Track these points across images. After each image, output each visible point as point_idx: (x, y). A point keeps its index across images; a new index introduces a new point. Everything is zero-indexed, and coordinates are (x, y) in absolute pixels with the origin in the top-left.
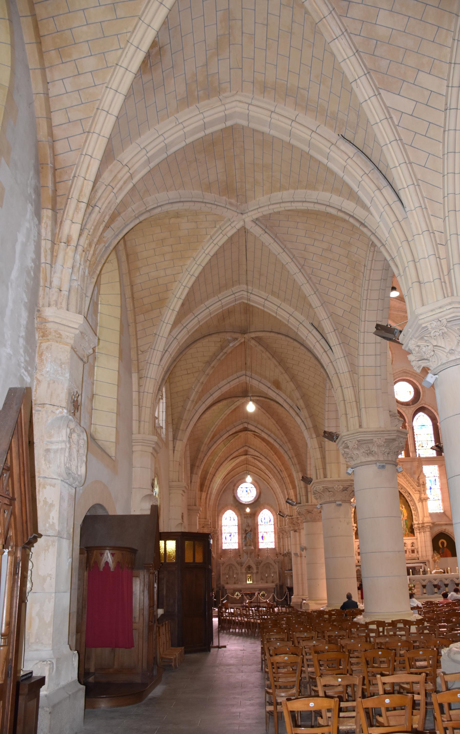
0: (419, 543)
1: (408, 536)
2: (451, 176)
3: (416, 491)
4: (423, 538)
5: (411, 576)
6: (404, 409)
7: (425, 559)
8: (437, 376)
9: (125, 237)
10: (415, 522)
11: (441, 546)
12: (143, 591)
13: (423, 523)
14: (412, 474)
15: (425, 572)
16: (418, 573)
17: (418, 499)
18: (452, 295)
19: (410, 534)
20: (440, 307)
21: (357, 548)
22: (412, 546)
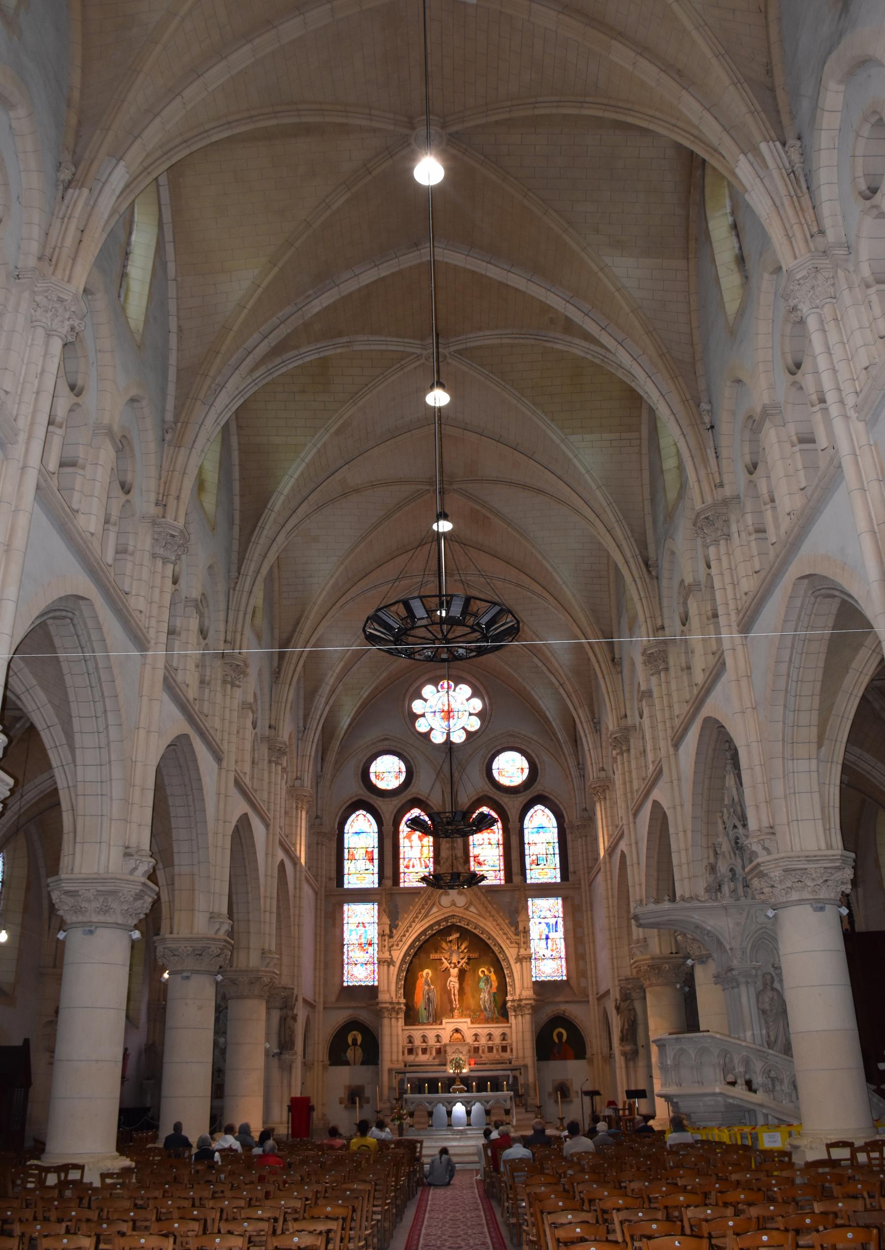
1: (497, 1022)
3: (511, 943)
4: (520, 1025)
7: (521, 1062)
9: (12, 665)
11: (556, 1040)
12: (85, 543)
13: (520, 1000)
17: (515, 957)
19: (501, 1018)
21: (406, 1040)
22: (504, 1039)
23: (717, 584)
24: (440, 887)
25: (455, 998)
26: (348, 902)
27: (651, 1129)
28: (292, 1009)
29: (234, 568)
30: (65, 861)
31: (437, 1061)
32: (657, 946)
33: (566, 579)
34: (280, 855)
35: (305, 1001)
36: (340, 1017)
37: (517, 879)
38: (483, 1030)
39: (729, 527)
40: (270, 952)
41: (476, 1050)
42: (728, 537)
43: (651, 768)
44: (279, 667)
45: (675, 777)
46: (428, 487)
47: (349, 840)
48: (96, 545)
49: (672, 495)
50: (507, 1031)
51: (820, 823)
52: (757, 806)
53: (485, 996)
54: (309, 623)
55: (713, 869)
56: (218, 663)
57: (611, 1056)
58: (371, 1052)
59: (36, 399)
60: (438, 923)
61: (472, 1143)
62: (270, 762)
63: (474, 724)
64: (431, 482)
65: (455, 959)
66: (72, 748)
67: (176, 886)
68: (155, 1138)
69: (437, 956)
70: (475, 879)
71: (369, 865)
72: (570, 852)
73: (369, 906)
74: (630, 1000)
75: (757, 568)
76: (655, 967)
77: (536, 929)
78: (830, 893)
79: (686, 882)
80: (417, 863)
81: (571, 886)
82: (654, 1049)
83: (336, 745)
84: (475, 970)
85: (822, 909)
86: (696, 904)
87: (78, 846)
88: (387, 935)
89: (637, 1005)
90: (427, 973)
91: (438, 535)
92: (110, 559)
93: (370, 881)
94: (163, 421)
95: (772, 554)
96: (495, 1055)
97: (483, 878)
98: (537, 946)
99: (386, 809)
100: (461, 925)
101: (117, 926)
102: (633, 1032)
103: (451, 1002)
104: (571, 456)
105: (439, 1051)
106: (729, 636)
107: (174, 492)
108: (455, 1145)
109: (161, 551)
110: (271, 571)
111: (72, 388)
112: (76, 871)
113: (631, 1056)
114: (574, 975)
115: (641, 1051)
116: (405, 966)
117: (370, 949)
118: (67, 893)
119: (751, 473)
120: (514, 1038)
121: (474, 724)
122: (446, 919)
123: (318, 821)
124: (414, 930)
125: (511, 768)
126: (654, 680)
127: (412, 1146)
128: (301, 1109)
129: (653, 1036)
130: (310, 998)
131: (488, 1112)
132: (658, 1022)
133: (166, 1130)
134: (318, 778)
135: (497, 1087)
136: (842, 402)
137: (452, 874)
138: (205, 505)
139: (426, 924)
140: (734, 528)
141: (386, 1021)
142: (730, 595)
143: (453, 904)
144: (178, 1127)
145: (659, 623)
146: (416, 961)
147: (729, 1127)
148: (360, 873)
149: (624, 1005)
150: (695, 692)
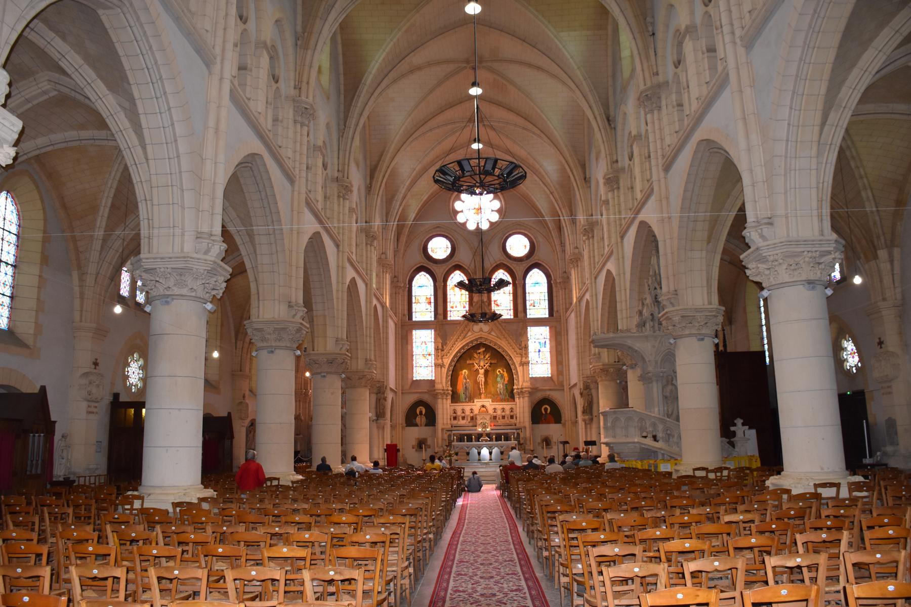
2: (169, 141)
7: (522, 425)
23: (651, 139)
24: (474, 321)
25: (482, 387)
26: (416, 329)
27: (598, 462)
28: (384, 393)
29: (342, 123)
30: (253, 312)
31: (471, 424)
32: (606, 357)
33: (555, 123)
34: (375, 302)
35: (391, 389)
36: (411, 399)
37: (521, 315)
38: (499, 406)
39: (660, 102)
40: (342, 339)
41: (495, 417)
42: (659, 108)
43: (607, 249)
44: (371, 183)
45: (620, 256)
46: (464, 65)
47: (415, 291)
48: (262, 120)
49: (626, 74)
50: (514, 406)
51: (705, 289)
52: (668, 278)
53: (500, 386)
54: (389, 155)
55: (640, 313)
56: (335, 185)
57: (576, 422)
58: (431, 418)
59: (225, 33)
60: (472, 342)
61: (493, 469)
62: (367, 244)
63: (495, 217)
64: (467, 61)
65: (482, 364)
66: (254, 245)
67: (315, 323)
68: (310, 466)
69: (471, 362)
70: (495, 317)
71: (428, 306)
72: (555, 299)
73: (429, 331)
74: (589, 391)
75: (677, 129)
76: (605, 370)
77: (532, 346)
78: (709, 331)
79: (625, 320)
80: (458, 305)
81: (555, 319)
82: (602, 418)
83: (406, 231)
84: (494, 370)
85: (703, 339)
86: (629, 334)
87: (261, 302)
88: (440, 350)
89: (594, 392)
90: (465, 372)
91: (473, 98)
92: (270, 127)
93: (429, 316)
94: (296, 32)
95: (686, 123)
96: (506, 421)
97: (501, 316)
98: (532, 355)
99: (439, 272)
100: (484, 346)
101: (287, 348)
102: (589, 408)
103: (479, 389)
104: (561, 46)
105: (472, 418)
106: (657, 174)
107: (305, 80)
108: (481, 471)
109: (299, 119)
110: (364, 127)
111: (241, 18)
112: (261, 316)
113: (589, 422)
114: (555, 373)
115: (595, 419)
116: (451, 368)
117: (430, 358)
118: (256, 329)
119: (676, 67)
120: (518, 411)
121: (495, 217)
122: (476, 340)
123: (396, 279)
124: (457, 347)
125: (518, 246)
126: (610, 195)
127: (459, 471)
128: (392, 451)
129: (601, 410)
130: (393, 388)
131: (502, 453)
132: (604, 403)
133: (317, 462)
134: (396, 252)
135: (507, 438)
136: (733, 33)
137: (479, 314)
138: (323, 83)
139: (464, 342)
140: (664, 103)
141: (440, 401)
142: (659, 146)
143: (481, 330)
144: (324, 460)
145: (615, 159)
146: (458, 365)
147: (642, 460)
148: (423, 311)
149: (585, 392)
150: (636, 204)
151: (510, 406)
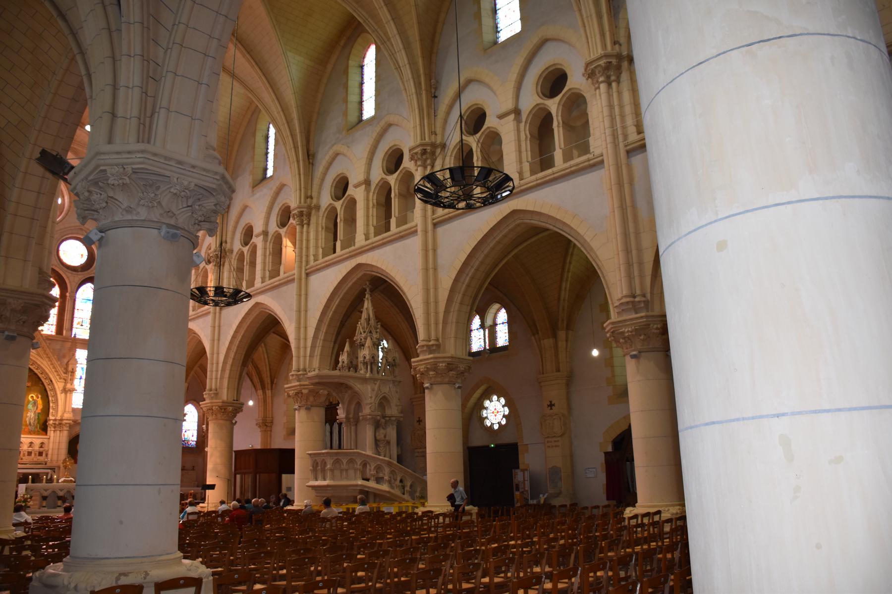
0: (51, 445)
5: (30, 484)
6: (69, 275)
7: (54, 464)
8: (103, 234)
10: (51, 417)
13: (61, 420)
14: (60, 358)
15: (50, 481)
16: (41, 481)
18: (149, 142)
20: (129, 152)
22: (41, 447)
50: (46, 441)
145: (309, 194)
151: (40, 441)
